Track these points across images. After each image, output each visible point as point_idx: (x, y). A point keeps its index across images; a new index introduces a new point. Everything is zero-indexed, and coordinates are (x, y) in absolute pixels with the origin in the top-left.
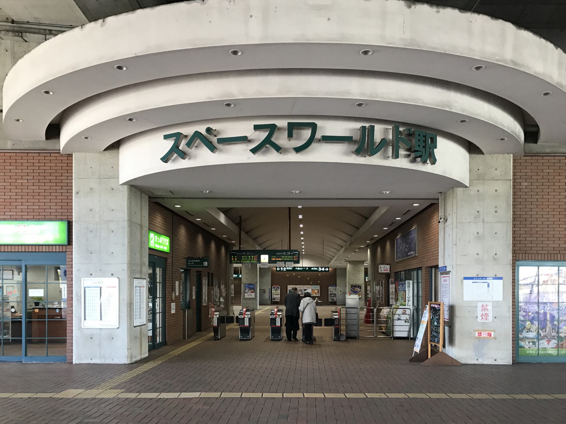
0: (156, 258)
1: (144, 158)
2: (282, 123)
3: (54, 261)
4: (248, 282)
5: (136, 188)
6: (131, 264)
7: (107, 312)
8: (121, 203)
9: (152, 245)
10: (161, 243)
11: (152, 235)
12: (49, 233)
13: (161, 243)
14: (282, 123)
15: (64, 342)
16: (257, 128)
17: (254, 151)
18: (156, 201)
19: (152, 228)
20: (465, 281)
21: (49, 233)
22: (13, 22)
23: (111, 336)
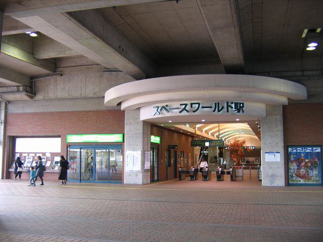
0: (154, 146)
1: (148, 114)
2: (188, 103)
3: (119, 147)
4: (229, 157)
5: (145, 123)
6: (293, 98)
7: (134, 163)
8: (140, 128)
9: (152, 141)
10: (156, 139)
11: (152, 137)
12: (116, 138)
13: (156, 139)
14: (188, 103)
15: (121, 180)
16: (181, 105)
17: (180, 112)
18: (152, 127)
19: (152, 134)
20: (266, 154)
21: (116, 138)
22: (106, 68)
23: (136, 174)
